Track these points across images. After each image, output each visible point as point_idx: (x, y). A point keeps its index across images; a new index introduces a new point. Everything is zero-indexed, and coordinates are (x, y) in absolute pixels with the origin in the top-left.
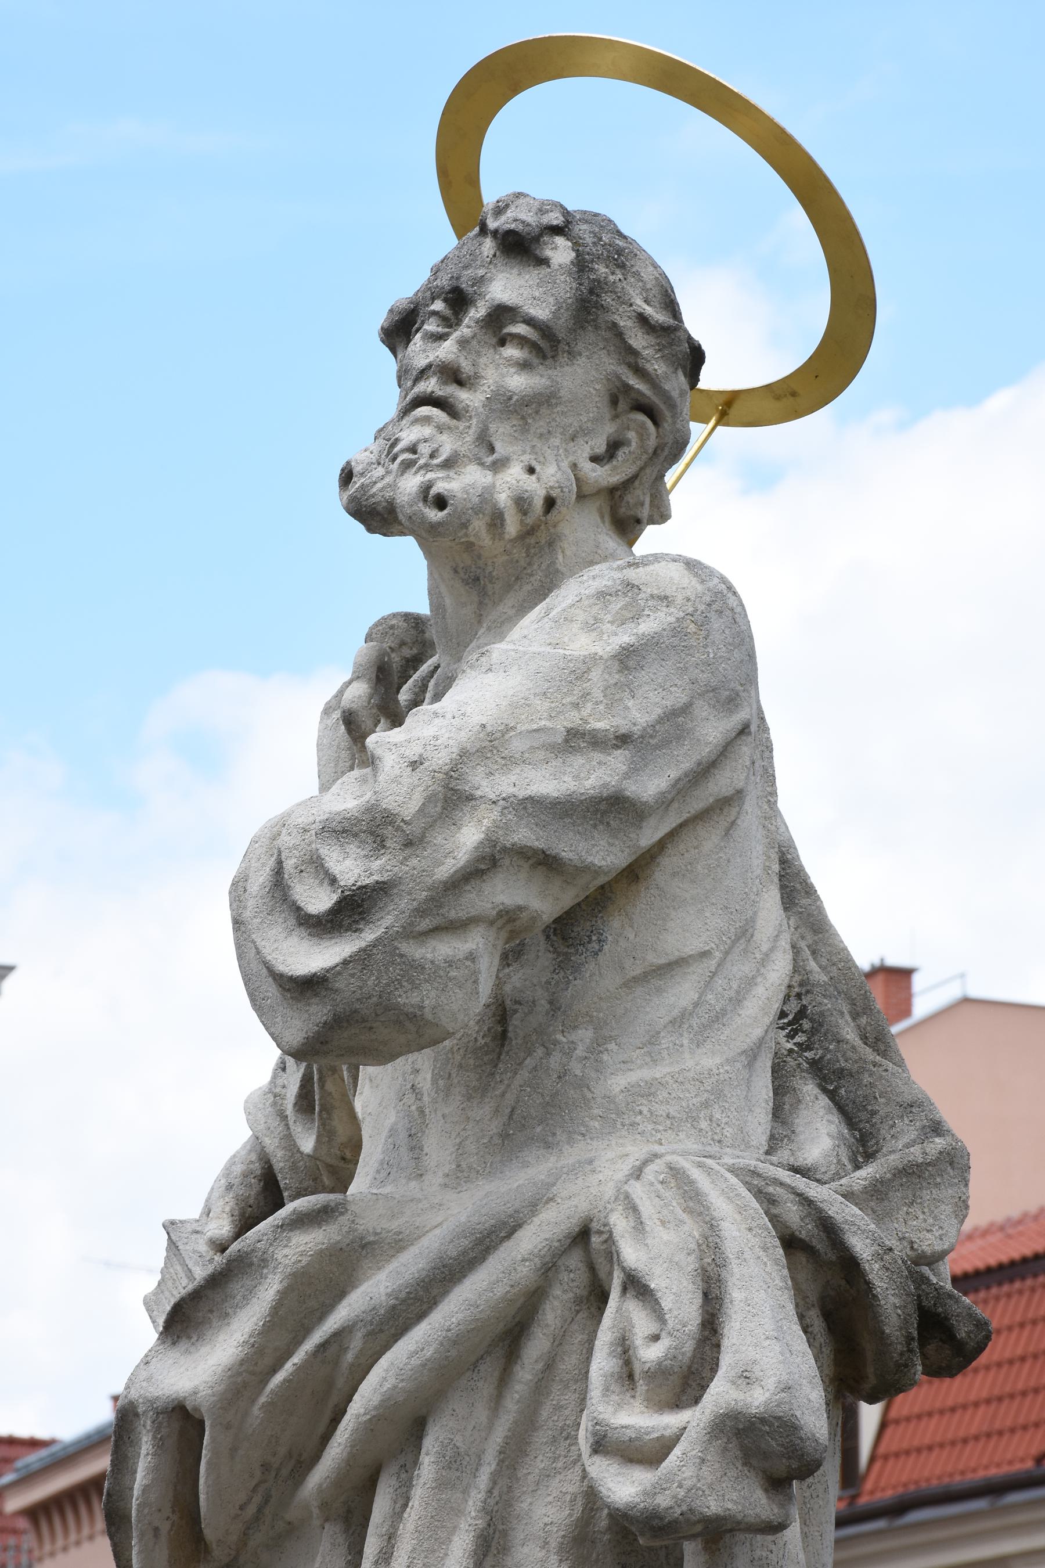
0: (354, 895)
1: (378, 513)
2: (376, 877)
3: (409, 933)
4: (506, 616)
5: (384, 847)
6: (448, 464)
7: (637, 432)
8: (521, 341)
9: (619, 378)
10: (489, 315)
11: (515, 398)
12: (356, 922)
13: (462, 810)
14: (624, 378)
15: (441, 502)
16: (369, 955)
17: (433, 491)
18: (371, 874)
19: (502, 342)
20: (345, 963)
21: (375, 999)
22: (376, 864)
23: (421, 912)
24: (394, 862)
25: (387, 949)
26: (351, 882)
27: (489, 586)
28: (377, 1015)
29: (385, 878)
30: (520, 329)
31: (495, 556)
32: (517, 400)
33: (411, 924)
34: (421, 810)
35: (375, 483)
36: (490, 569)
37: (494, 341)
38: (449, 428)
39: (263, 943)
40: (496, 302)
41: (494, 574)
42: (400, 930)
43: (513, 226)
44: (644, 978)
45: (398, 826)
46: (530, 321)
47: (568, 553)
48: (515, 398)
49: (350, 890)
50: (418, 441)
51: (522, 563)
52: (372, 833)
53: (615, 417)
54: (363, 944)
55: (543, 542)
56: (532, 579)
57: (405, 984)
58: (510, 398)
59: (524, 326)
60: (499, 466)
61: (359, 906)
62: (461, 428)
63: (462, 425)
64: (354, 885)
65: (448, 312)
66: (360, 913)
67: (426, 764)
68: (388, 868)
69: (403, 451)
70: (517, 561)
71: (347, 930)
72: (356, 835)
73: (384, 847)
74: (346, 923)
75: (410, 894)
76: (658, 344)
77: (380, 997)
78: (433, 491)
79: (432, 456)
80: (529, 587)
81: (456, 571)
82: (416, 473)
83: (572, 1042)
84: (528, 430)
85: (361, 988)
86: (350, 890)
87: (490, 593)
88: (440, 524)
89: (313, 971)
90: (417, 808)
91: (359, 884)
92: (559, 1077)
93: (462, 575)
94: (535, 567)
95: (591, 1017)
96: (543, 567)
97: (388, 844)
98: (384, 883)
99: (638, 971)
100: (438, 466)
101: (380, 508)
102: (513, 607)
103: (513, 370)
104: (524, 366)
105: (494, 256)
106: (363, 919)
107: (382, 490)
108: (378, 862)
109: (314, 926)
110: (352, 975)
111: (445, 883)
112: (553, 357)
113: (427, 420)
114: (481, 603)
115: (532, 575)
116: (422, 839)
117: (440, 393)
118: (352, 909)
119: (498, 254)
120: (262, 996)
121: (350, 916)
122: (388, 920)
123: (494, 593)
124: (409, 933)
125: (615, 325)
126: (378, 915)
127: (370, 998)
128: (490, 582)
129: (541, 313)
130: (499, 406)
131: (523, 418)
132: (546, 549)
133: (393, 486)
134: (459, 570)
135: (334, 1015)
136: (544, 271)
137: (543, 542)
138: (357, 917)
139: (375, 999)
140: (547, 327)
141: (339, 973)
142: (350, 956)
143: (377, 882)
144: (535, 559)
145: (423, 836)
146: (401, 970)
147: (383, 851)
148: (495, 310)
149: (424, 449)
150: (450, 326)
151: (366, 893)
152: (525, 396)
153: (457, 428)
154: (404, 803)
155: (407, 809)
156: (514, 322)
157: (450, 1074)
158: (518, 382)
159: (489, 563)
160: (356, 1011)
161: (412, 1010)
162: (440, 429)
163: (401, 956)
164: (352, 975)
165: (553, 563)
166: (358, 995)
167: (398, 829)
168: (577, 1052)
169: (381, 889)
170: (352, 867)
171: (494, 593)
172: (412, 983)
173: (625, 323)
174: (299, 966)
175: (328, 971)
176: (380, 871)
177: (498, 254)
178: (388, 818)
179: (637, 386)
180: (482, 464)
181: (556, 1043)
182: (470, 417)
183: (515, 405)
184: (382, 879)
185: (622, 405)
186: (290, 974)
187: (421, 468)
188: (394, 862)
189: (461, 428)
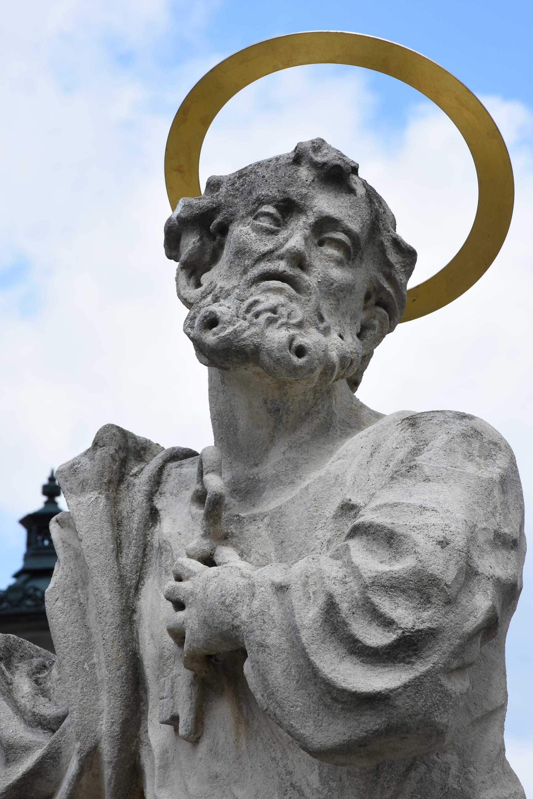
0: (412, 636)
1: (245, 353)
2: (427, 625)
3: (448, 671)
4: (303, 440)
5: (430, 602)
6: (300, 325)
7: (380, 321)
8: (338, 244)
9: (377, 281)
10: (316, 223)
11: (335, 285)
12: (410, 656)
13: (473, 582)
14: (381, 281)
15: (300, 351)
16: (421, 683)
17: (295, 343)
18: (423, 622)
19: (321, 243)
20: (405, 686)
21: (421, 716)
22: (426, 615)
23: (455, 655)
24: (439, 615)
25: (434, 680)
26: (410, 625)
27: (285, 416)
28: (418, 729)
29: (434, 625)
30: (340, 236)
31: (297, 396)
32: (337, 287)
33: (449, 663)
34: (456, 578)
35: (245, 330)
36: (290, 404)
37: (316, 241)
38: (297, 299)
39: (322, 664)
40: (325, 214)
41: (291, 408)
42: (442, 666)
43: (339, 162)
44: (479, 721)
45: (443, 588)
46: (347, 232)
47: (338, 400)
48: (335, 285)
49: (410, 632)
50: (278, 305)
51: (310, 403)
52: (419, 591)
53: (365, 309)
54: (418, 674)
55: (324, 390)
56: (319, 415)
57: (441, 707)
58: (332, 284)
59: (343, 235)
60: (326, 331)
61: (415, 644)
62: (303, 300)
63: (303, 298)
64: (412, 628)
65: (278, 215)
66: (414, 650)
67: (452, 544)
68: (436, 618)
69: (266, 310)
70: (308, 401)
71: (400, 662)
72: (404, 591)
73: (430, 602)
74: (402, 655)
75: (449, 640)
76: (404, 262)
77: (425, 715)
78: (295, 343)
79: (289, 315)
80: (318, 421)
81: (266, 402)
82: (279, 328)
83: (447, 763)
84: (338, 309)
85: (413, 707)
86: (410, 632)
87: (284, 421)
88: (301, 367)
89: (378, 690)
90: (454, 577)
91: (416, 628)
92: (442, 789)
93: (269, 405)
94: (320, 407)
95: (454, 745)
96: (325, 408)
97: (433, 600)
98: (434, 629)
99: (479, 715)
100: (294, 325)
101: (248, 349)
102: (308, 433)
103: (332, 264)
104: (340, 263)
105: (313, 181)
106: (416, 655)
107: (251, 336)
108: (426, 614)
109: (369, 655)
110: (409, 697)
111: (469, 634)
112: (353, 260)
113: (280, 291)
114: (275, 427)
115: (319, 413)
116: (456, 599)
117: (291, 273)
118: (407, 647)
119: (316, 180)
120: (291, 704)
121: (406, 651)
122: (435, 658)
123: (287, 422)
124: (448, 671)
125: (382, 243)
126: (428, 653)
127: (417, 715)
128: (286, 413)
129: (355, 227)
130: (325, 288)
131: (338, 300)
132: (326, 395)
133: (262, 334)
134: (269, 402)
135: (388, 725)
136: (353, 198)
137: (324, 390)
138: (410, 653)
139: (421, 716)
140: (358, 238)
141: (400, 694)
142: (409, 682)
143: (429, 628)
144: (319, 401)
145: (456, 598)
146: (440, 696)
147: (429, 605)
148: (321, 220)
149: (282, 311)
150: (279, 226)
151: (421, 635)
152: (342, 284)
153: (301, 300)
154: (443, 571)
155: (448, 576)
156: (335, 230)
157: (340, 778)
158: (337, 274)
159: (291, 400)
160: (405, 724)
161: (442, 728)
162: (291, 298)
163: (441, 686)
164: (409, 697)
165: (331, 406)
166: (410, 712)
167: (442, 590)
168: (452, 770)
169: (432, 634)
170: (406, 615)
171: (287, 422)
172: (445, 707)
173: (387, 244)
174: (360, 685)
175: (391, 691)
176: (430, 620)
177: (316, 180)
178: (434, 581)
179: (388, 289)
180: (318, 328)
181: (434, 762)
182: (310, 293)
183: (335, 289)
184: (432, 626)
185: (372, 301)
186: (354, 690)
187: (283, 325)
188: (439, 615)
189: (303, 300)
